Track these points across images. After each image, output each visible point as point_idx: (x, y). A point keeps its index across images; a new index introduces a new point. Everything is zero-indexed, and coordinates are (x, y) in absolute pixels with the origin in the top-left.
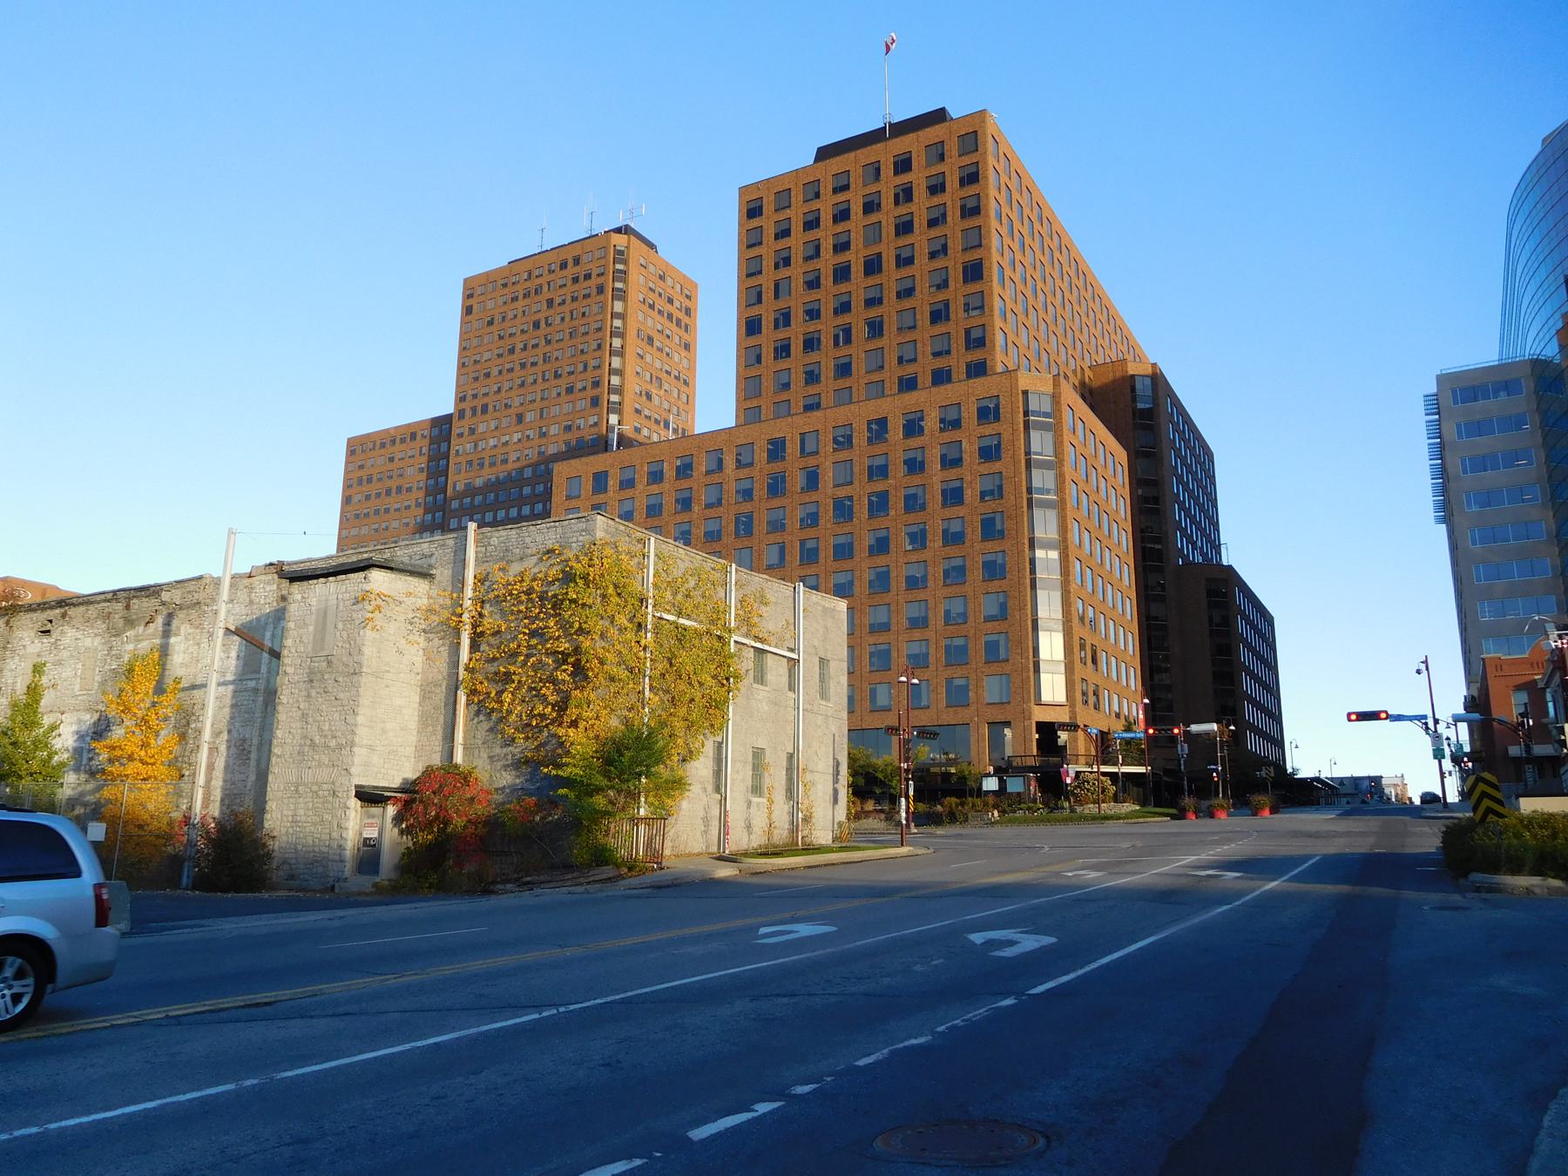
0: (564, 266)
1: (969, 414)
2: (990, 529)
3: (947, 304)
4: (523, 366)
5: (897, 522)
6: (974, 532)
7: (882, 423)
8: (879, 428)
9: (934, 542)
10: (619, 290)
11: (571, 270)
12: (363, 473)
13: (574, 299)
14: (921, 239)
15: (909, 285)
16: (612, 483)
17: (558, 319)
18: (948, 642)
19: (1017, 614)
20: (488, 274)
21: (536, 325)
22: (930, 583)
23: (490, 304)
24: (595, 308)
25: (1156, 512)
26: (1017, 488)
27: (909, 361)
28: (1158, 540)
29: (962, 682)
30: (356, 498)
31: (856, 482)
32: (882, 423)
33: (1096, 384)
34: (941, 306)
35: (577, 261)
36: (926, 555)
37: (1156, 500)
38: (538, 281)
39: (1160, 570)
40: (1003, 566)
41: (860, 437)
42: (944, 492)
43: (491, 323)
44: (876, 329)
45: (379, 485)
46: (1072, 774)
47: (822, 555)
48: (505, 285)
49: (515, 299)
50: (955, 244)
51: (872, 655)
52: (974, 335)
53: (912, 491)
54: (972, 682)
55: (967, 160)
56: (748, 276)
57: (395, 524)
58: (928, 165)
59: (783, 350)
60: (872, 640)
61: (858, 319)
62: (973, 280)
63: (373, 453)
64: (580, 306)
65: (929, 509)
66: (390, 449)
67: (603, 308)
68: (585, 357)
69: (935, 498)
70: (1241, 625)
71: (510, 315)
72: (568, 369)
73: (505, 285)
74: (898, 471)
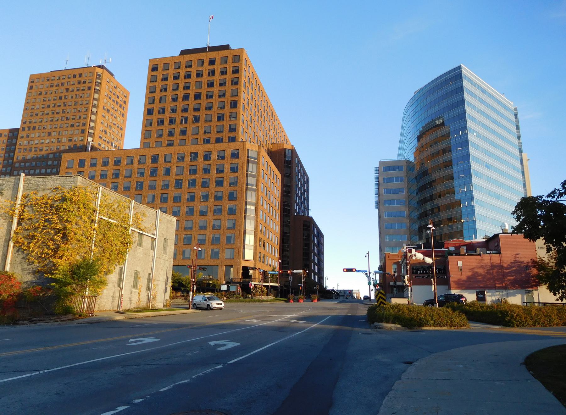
0: (74, 76)
1: (228, 155)
5: (198, 190)
6: (226, 197)
7: (196, 154)
8: (195, 156)
11: (78, 79)
13: (78, 90)
14: (216, 90)
20: (41, 74)
21: (60, 98)
22: (209, 214)
23: (41, 87)
24: (86, 95)
28: (289, 206)
29: (217, 250)
31: (184, 174)
32: (196, 154)
33: (273, 150)
35: (80, 76)
36: (208, 203)
37: (289, 192)
38: (63, 81)
39: (289, 216)
40: (235, 210)
43: (40, 94)
44: (197, 119)
46: (253, 285)
48: (48, 80)
49: (52, 86)
51: (185, 238)
54: (221, 251)
58: (221, 64)
60: (185, 233)
61: (190, 115)
64: (80, 93)
65: (211, 187)
67: (90, 96)
69: (213, 183)
73: (48, 80)
74: (200, 172)
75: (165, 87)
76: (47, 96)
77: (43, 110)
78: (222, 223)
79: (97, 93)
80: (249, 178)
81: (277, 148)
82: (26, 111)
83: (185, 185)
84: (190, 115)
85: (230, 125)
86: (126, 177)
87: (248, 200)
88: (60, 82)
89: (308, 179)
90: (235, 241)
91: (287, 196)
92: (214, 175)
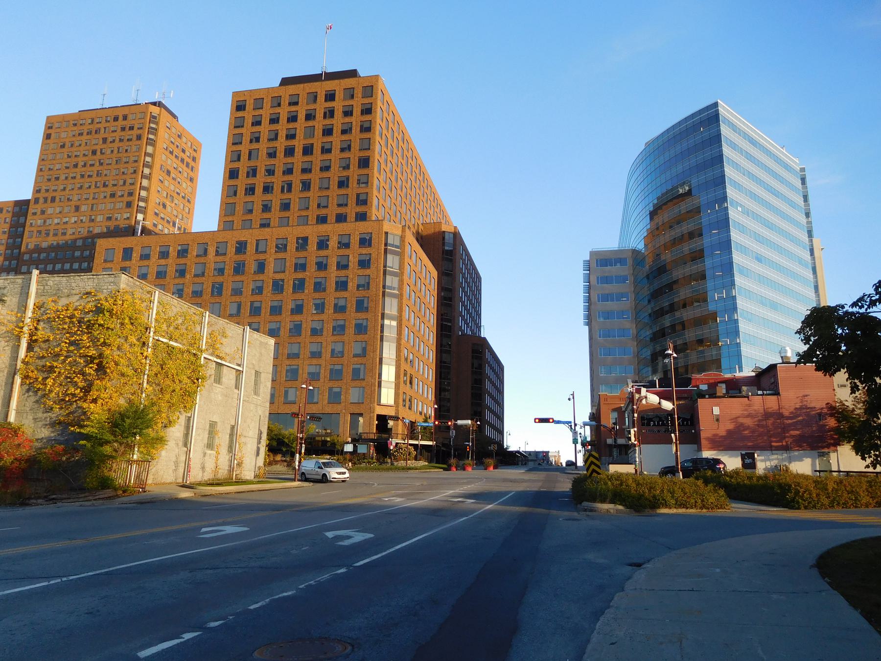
0: (116, 119)
1: (355, 241)
2: (361, 306)
5: (308, 296)
6: (351, 307)
7: (305, 239)
11: (121, 123)
13: (121, 140)
18: (332, 367)
20: (64, 116)
21: (94, 153)
22: (325, 333)
24: (134, 148)
27: (324, 207)
29: (338, 390)
32: (305, 239)
33: (425, 233)
35: (125, 118)
36: (323, 317)
37: (450, 299)
38: (98, 126)
40: (366, 327)
41: (292, 246)
43: (63, 146)
44: (306, 186)
46: (394, 444)
48: (75, 125)
49: (81, 134)
51: (287, 371)
58: (345, 99)
60: (288, 362)
61: (296, 179)
64: (124, 145)
65: (328, 291)
67: (139, 149)
71: (77, 144)
73: (75, 125)
74: (312, 268)
76: (74, 149)
77: (67, 171)
78: (346, 347)
79: (151, 145)
81: (431, 231)
82: (41, 173)
83: (289, 288)
84: (296, 179)
85: (358, 195)
88: (94, 127)
90: (367, 375)
92: (333, 274)
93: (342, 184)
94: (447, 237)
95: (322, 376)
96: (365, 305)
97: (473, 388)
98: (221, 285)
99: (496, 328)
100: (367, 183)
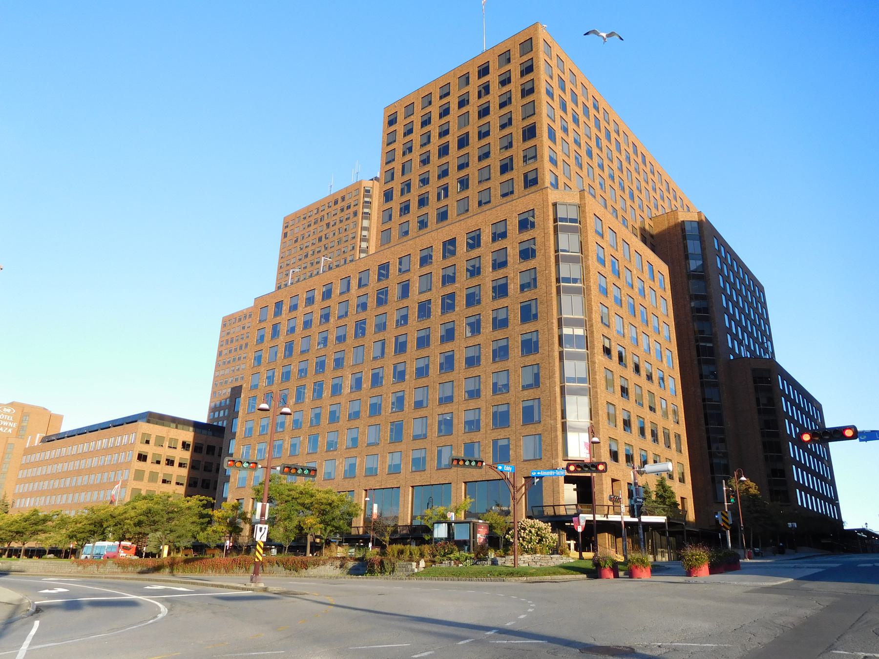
0: (336, 203)
1: (513, 226)
2: (528, 314)
3: (511, 158)
4: (312, 264)
5: (461, 313)
6: (515, 317)
7: (453, 242)
8: (450, 246)
9: (487, 327)
10: (367, 213)
11: (340, 204)
12: (229, 337)
13: (341, 221)
14: (494, 118)
15: (487, 151)
16: (285, 308)
17: (332, 234)
18: (495, 409)
19: (547, 382)
20: (296, 213)
21: (320, 239)
22: (483, 362)
23: (296, 230)
24: (352, 225)
25: (707, 319)
26: (548, 279)
27: (485, 203)
28: (709, 340)
29: (505, 442)
30: (224, 352)
31: (434, 289)
32: (453, 242)
33: (655, 231)
34: (507, 161)
35: (343, 199)
36: (479, 339)
37: (706, 310)
38: (322, 213)
39: (713, 362)
40: (537, 343)
41: (437, 254)
42: (494, 288)
43: (296, 241)
44: (464, 183)
45: (237, 343)
46: (583, 523)
47: (409, 346)
48: (305, 218)
49: (309, 226)
50: (517, 117)
51: (440, 423)
52: (530, 177)
53: (471, 291)
54: (512, 442)
55: (526, 58)
56: (387, 163)
57: (243, 366)
58: (500, 66)
59: (405, 209)
60: (440, 410)
61: (452, 180)
62: (529, 139)
63: (235, 325)
64: (343, 226)
65: (483, 303)
66: (243, 322)
67: (356, 225)
68: (345, 255)
69: (487, 293)
70: (784, 405)
71: (307, 235)
72: (335, 264)
73: (305, 218)
74: (462, 276)
75: (409, 145)
76: (305, 241)
77: (300, 263)
78: (512, 377)
79: (366, 218)
80: (562, 265)
81: (664, 226)
82: (282, 270)
83: (436, 308)
84: (452, 180)
85: (526, 176)
86: (340, 318)
87: (564, 316)
88: (318, 216)
89: (761, 289)
90: (538, 415)
91: (701, 319)
92: (488, 276)
93: (505, 168)
94: (688, 228)
95: (482, 424)
96: (533, 312)
97: (763, 435)
98: (364, 322)
99: (801, 350)
100: (535, 157)
